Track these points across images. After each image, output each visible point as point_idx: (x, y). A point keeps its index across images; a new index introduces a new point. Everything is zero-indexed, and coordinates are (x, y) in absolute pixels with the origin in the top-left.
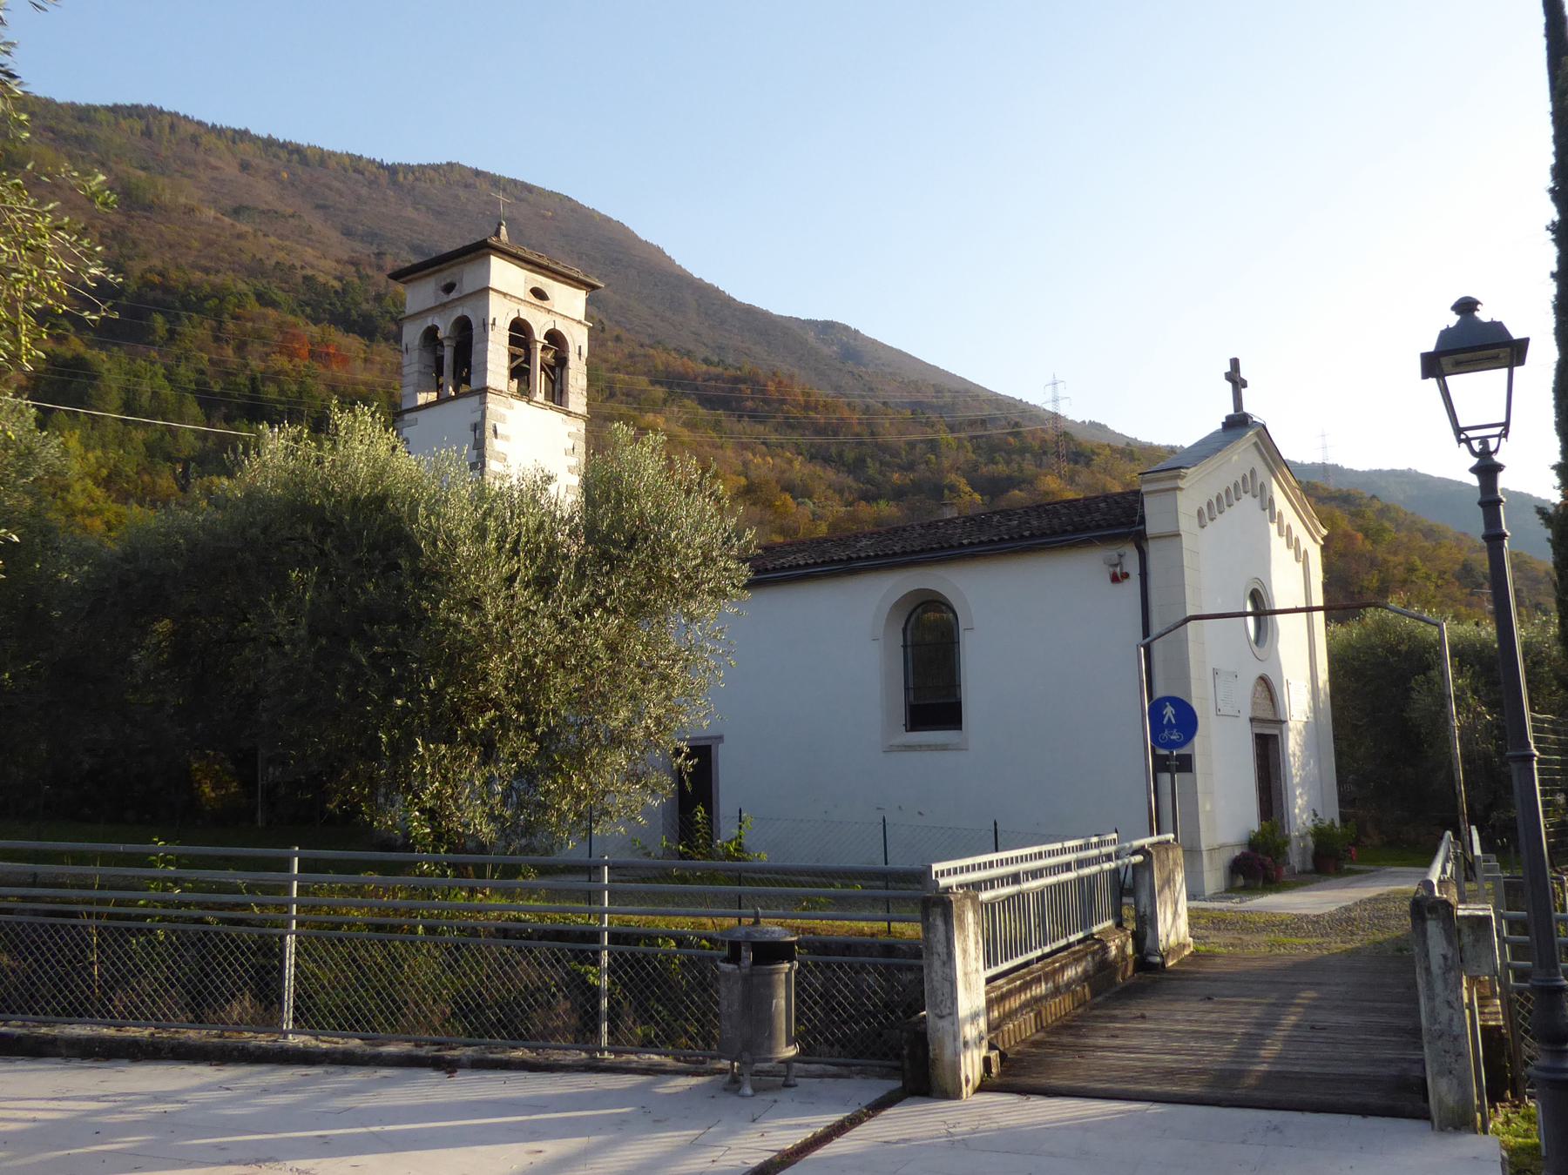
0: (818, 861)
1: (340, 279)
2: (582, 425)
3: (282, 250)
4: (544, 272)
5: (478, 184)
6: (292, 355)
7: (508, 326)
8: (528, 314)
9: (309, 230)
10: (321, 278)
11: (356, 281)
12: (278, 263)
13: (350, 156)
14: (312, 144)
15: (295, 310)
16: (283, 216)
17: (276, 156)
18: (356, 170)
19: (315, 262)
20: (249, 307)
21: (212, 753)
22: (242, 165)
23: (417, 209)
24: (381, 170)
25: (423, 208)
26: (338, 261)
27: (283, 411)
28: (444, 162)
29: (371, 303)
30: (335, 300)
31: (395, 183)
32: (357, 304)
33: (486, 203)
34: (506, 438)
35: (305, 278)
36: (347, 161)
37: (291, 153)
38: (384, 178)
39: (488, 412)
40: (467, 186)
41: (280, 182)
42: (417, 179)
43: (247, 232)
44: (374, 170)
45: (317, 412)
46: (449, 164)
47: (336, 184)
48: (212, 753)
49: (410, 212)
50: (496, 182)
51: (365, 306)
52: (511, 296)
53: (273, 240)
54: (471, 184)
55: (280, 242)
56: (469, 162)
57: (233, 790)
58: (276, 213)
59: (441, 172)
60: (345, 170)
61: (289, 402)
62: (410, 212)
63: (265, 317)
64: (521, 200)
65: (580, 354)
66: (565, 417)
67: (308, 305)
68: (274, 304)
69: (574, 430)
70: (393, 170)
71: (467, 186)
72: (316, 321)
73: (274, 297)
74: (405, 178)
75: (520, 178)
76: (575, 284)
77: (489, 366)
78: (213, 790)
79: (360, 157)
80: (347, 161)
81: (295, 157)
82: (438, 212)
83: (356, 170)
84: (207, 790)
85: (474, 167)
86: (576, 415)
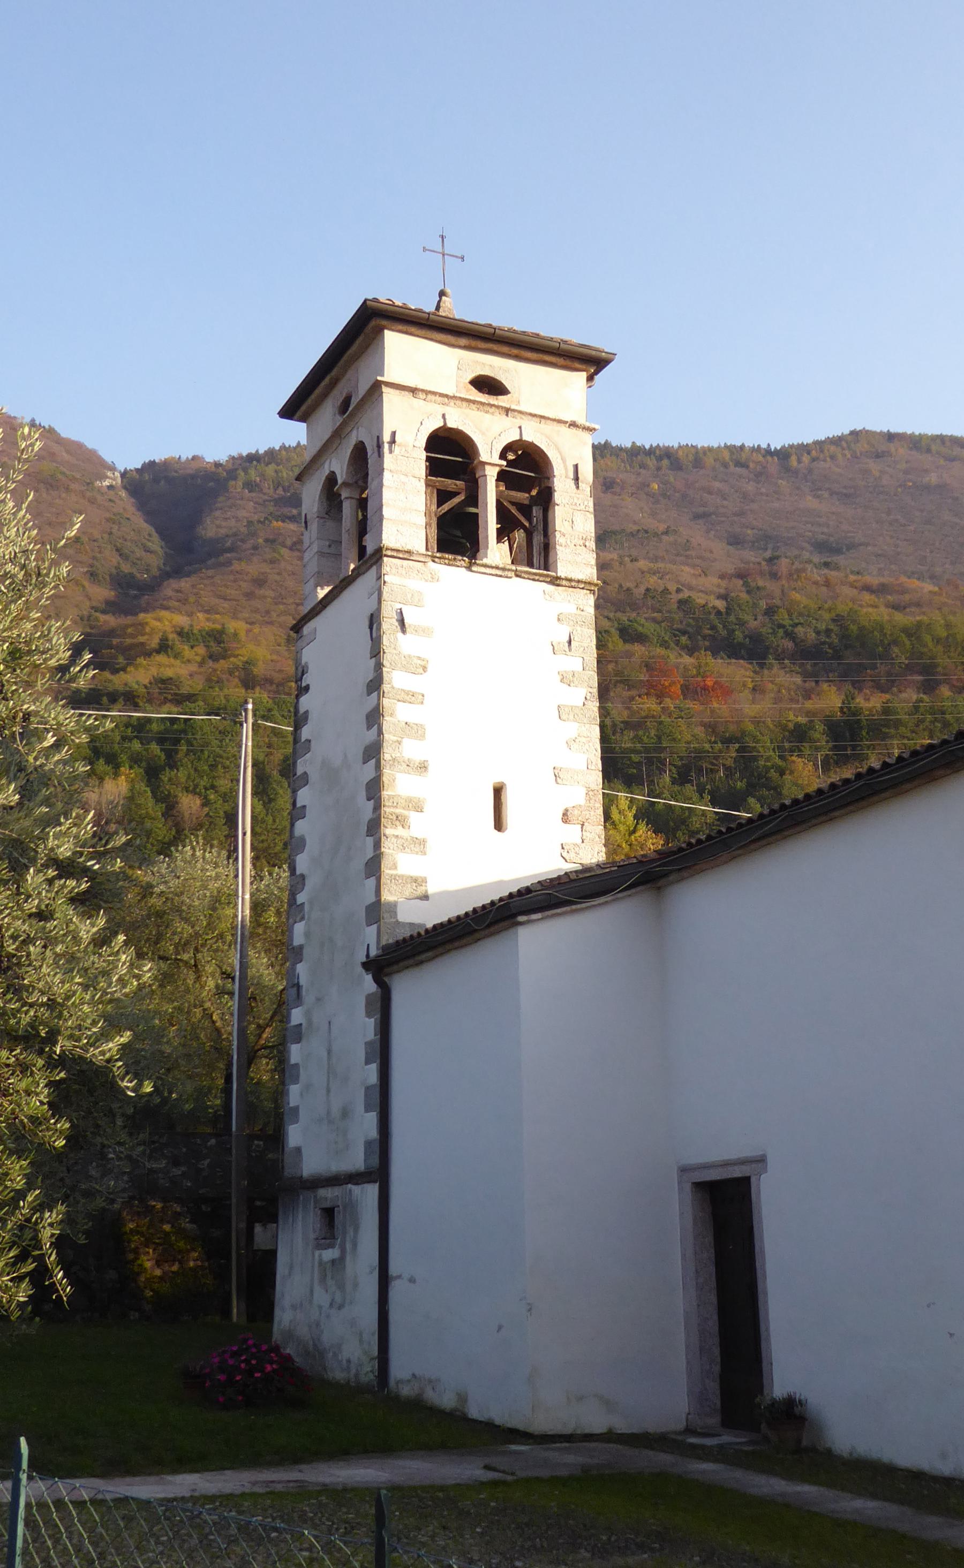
0: (944, 1456)
1: (724, 597)
2: (587, 602)
3: (654, 574)
4: (490, 346)
5: (893, 450)
6: (660, 696)
7: (422, 442)
8: (460, 419)
9: (687, 545)
10: (700, 599)
11: (744, 596)
12: (648, 590)
13: (731, 449)
14: (683, 443)
15: (666, 642)
16: (656, 535)
17: (643, 466)
18: (739, 464)
19: (694, 582)
20: (610, 645)
21: (159, 1206)
22: (604, 484)
23: (818, 497)
24: (769, 458)
25: (826, 495)
26: (722, 577)
27: (640, 763)
28: (847, 432)
29: (760, 617)
30: (716, 622)
31: (787, 469)
32: (742, 623)
33: (906, 472)
34: (425, 632)
35: (681, 602)
36: (727, 456)
37: (660, 459)
38: (773, 465)
39: (386, 590)
40: (878, 456)
41: (649, 495)
42: (814, 460)
43: (612, 560)
44: (761, 458)
45: (681, 758)
46: (853, 433)
47: (717, 485)
48: (159, 1206)
49: (810, 502)
50: (916, 443)
51: (753, 624)
52: (427, 392)
53: (642, 564)
54: (883, 452)
55: (652, 565)
56: (879, 424)
57: (192, 1264)
58: (646, 532)
59: (844, 444)
60: (725, 465)
61: (647, 750)
62: (810, 502)
63: (629, 655)
64: (952, 460)
65: (576, 479)
66: (550, 588)
67: (684, 633)
68: (640, 638)
69: (570, 608)
70: (783, 455)
71: (878, 456)
72: (691, 651)
73: (640, 629)
74: (799, 461)
75: (947, 431)
76: (560, 361)
77: (386, 512)
78: (158, 1264)
79: (742, 447)
80: (727, 456)
81: (665, 462)
82: (846, 495)
83: (739, 464)
84: (148, 1265)
85: (885, 430)
86: (573, 583)
